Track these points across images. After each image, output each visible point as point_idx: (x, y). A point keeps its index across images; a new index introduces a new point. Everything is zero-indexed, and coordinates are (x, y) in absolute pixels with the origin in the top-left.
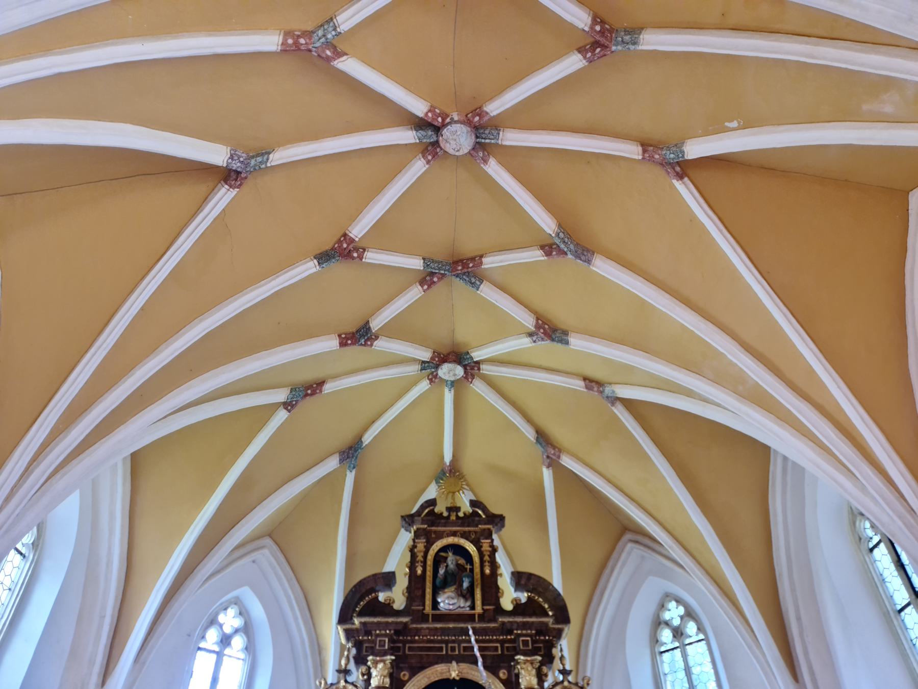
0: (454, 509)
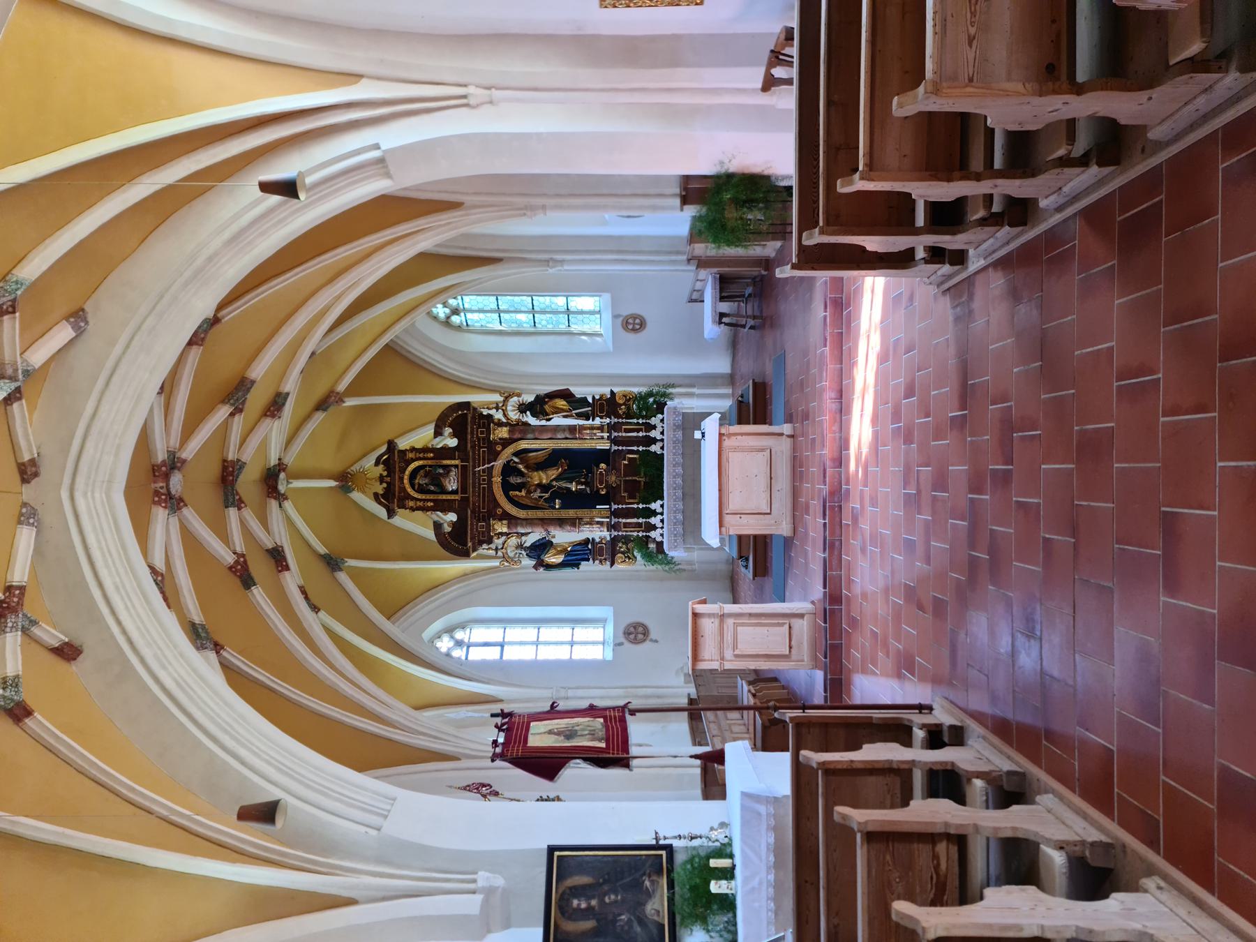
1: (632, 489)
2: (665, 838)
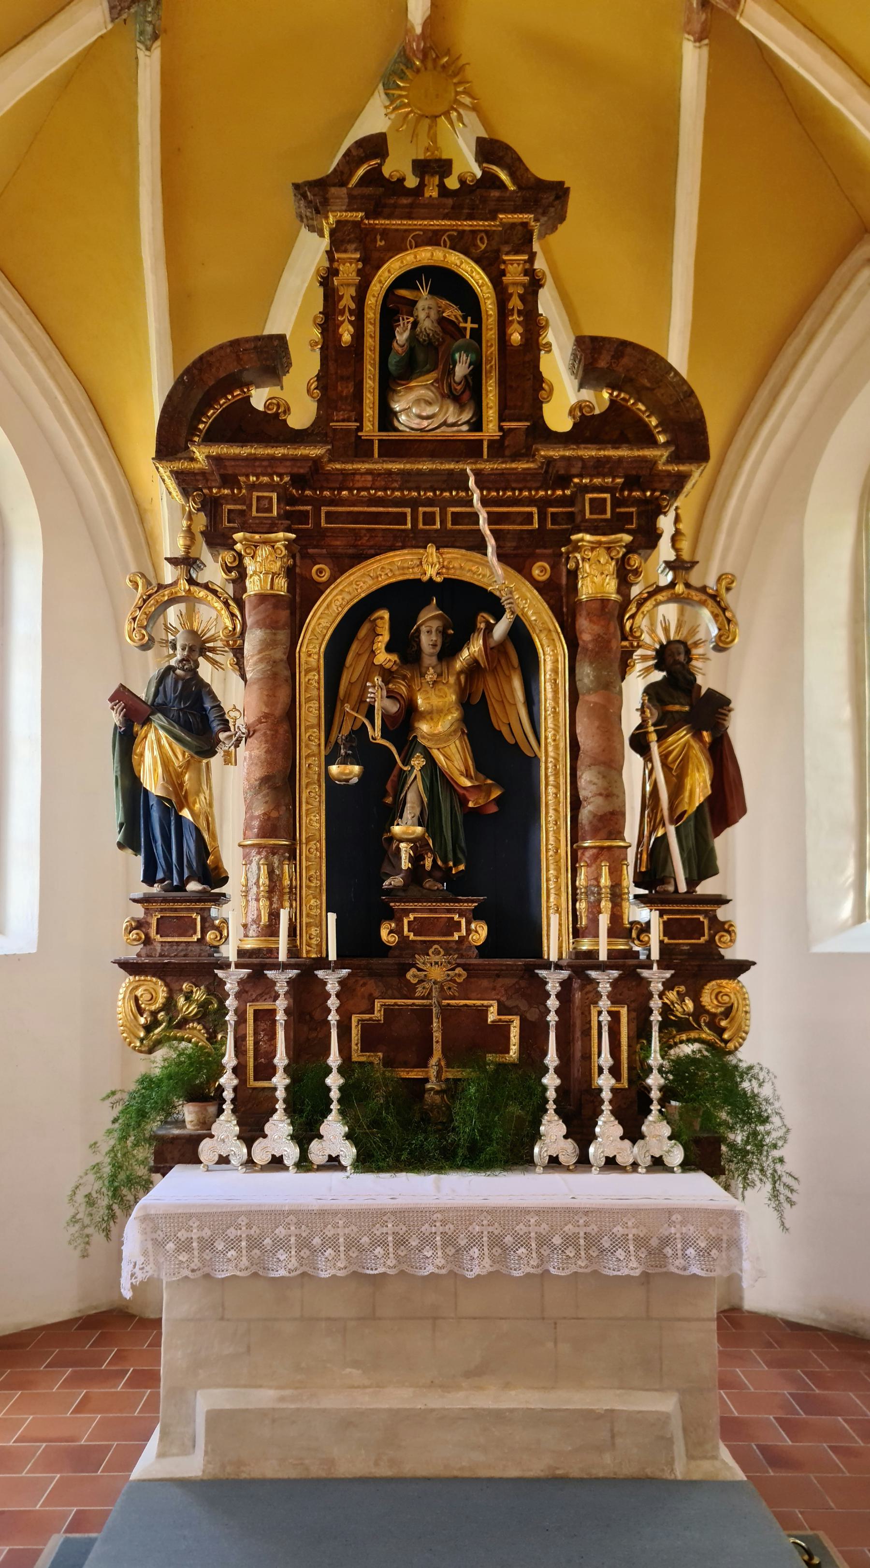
0: (434, 167)
1: (397, 1038)
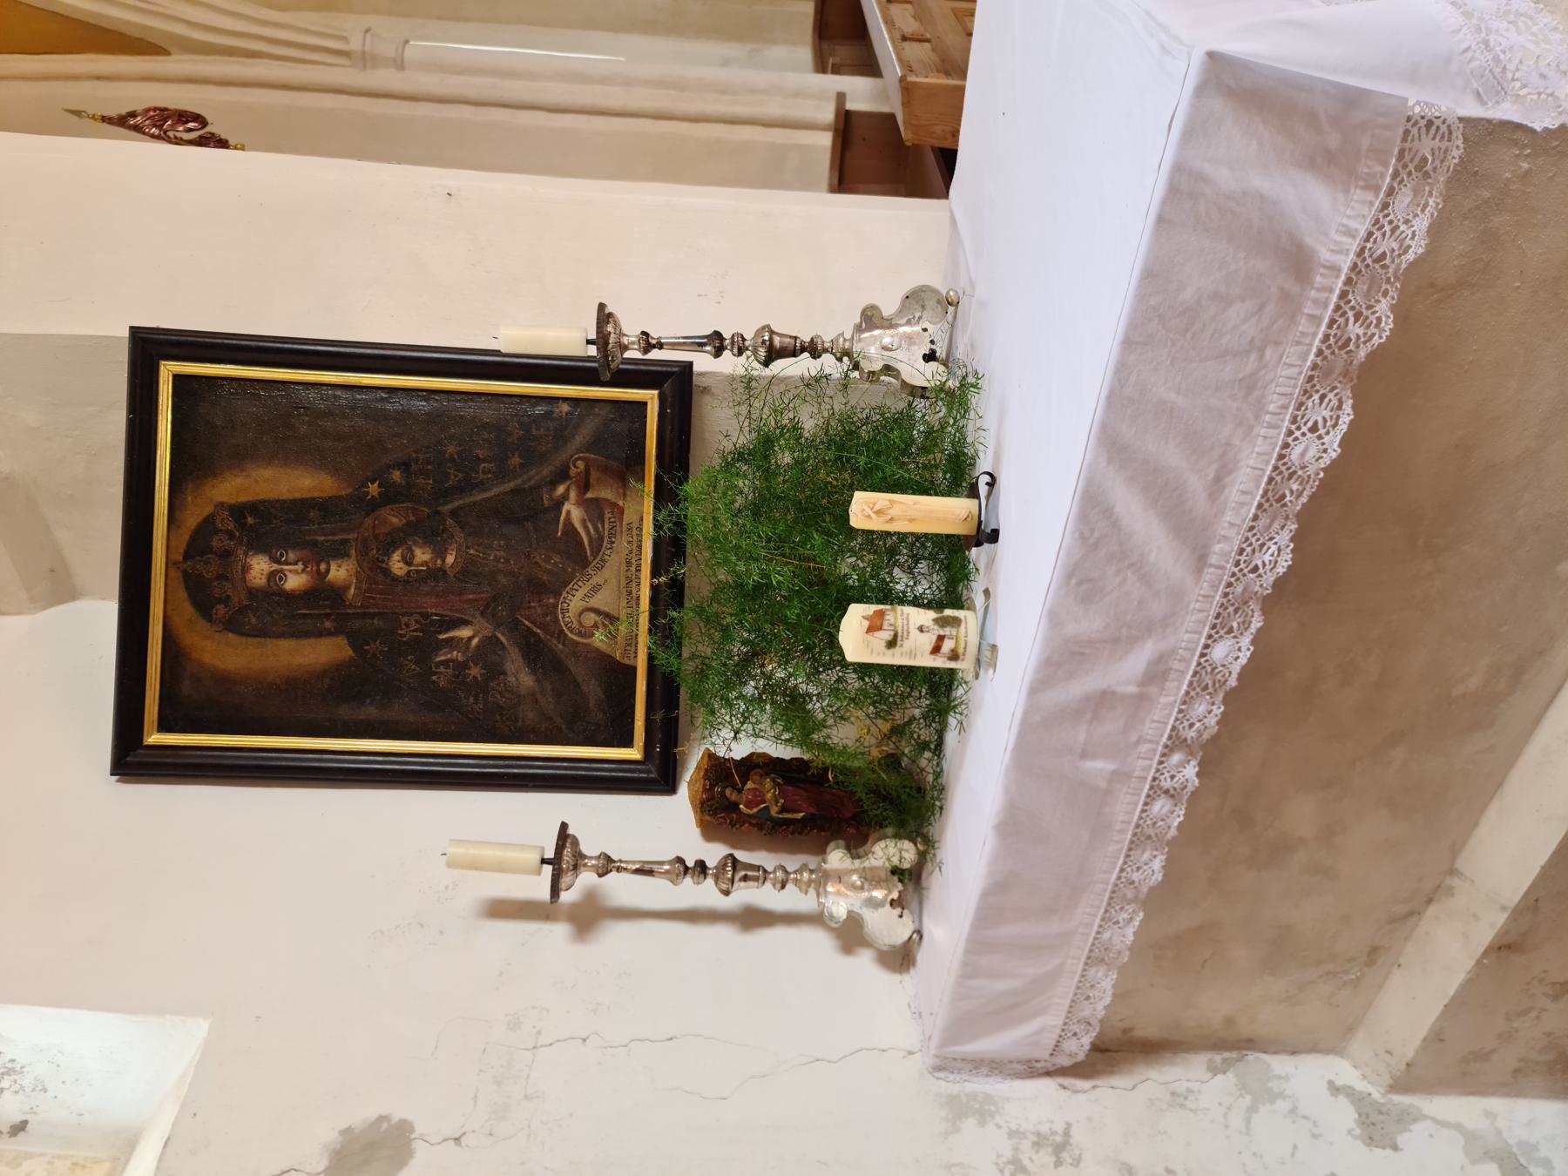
2: (648, 343)
